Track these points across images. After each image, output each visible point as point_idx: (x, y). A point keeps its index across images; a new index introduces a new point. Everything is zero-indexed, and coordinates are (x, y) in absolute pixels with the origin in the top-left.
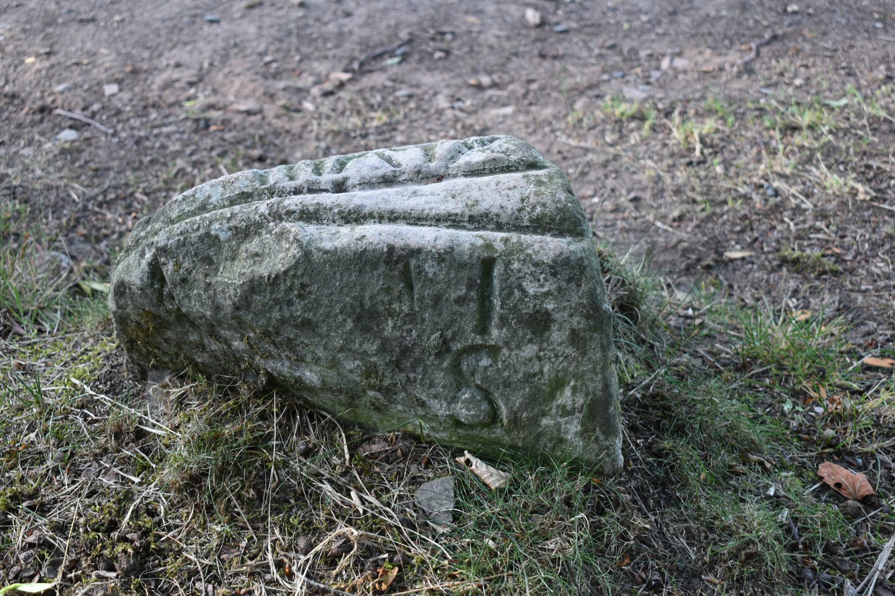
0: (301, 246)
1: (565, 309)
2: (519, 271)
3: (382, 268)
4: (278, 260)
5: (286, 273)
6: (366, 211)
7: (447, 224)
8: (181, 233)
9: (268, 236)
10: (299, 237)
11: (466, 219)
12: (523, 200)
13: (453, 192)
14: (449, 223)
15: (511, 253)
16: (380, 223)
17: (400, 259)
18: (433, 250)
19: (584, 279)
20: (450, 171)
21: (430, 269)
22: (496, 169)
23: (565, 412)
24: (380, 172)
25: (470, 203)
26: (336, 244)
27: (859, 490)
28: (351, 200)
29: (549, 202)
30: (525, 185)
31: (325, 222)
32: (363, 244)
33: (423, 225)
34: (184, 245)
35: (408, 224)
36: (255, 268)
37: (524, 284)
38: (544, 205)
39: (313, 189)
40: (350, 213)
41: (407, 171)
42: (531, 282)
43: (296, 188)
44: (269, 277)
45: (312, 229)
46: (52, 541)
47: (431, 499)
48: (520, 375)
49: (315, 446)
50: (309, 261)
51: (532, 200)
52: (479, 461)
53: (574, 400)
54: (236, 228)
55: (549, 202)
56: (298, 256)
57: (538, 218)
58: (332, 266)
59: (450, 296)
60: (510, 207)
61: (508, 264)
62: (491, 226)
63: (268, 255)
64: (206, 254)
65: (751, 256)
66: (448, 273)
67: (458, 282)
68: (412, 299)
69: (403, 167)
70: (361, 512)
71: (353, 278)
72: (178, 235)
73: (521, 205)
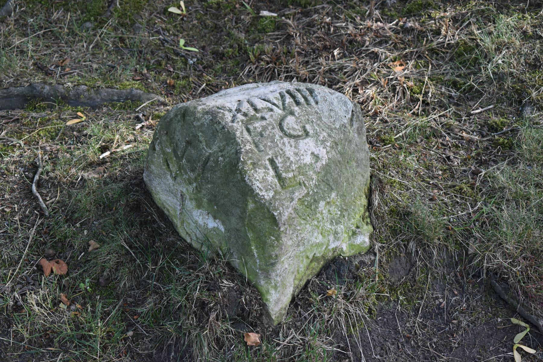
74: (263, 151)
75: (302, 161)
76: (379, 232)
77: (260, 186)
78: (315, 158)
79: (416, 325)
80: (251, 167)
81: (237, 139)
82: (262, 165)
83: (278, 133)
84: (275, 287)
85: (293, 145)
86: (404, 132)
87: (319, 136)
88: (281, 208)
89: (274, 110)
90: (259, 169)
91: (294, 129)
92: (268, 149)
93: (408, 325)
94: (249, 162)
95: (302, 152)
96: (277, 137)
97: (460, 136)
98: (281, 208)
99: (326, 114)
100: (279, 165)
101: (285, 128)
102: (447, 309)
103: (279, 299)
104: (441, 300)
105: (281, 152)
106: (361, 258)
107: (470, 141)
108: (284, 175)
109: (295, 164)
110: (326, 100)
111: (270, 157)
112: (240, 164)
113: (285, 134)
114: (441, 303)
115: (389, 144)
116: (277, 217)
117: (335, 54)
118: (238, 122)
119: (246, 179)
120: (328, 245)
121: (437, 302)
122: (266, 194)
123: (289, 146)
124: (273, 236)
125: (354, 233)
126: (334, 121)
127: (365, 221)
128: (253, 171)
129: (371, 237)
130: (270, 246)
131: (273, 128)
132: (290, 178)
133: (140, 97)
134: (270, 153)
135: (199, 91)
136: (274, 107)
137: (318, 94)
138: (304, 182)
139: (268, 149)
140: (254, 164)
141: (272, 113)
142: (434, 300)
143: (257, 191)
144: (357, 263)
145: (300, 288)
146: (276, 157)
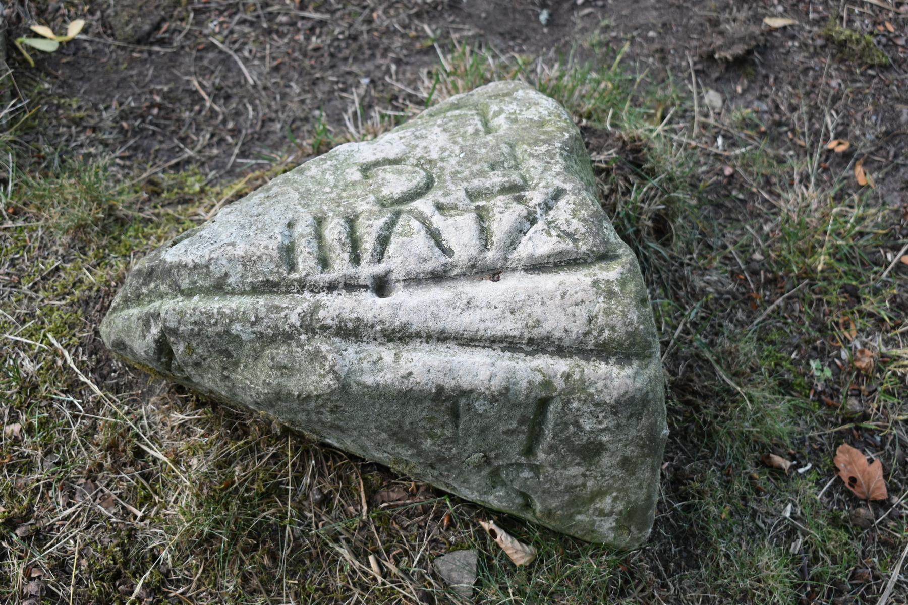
0: (338, 378)
1: (620, 440)
2: (578, 410)
3: (428, 403)
4: (310, 382)
5: (318, 396)
6: (413, 330)
7: (502, 346)
8: (195, 323)
9: (299, 350)
10: (336, 368)
11: (525, 341)
12: (590, 321)
13: (513, 306)
14: (505, 345)
15: (571, 391)
16: (428, 343)
17: (449, 398)
18: (487, 392)
19: (646, 412)
20: (509, 264)
21: (480, 406)
22: (561, 262)
23: (601, 513)
24: (429, 266)
25: (531, 323)
26: (378, 378)
27: (873, 492)
28: (396, 315)
29: (619, 325)
30: (593, 298)
31: (365, 339)
32: (409, 383)
33: (476, 346)
34: (199, 334)
35: (459, 344)
36: (283, 380)
37: (581, 421)
38: (613, 328)
39: (351, 286)
40: (394, 331)
41: (460, 264)
42: (589, 419)
43: (330, 283)
44: (299, 396)
45: (351, 351)
46: (54, 589)
47: (451, 570)
48: (562, 487)
49: (330, 492)
50: (347, 393)
51: (601, 320)
52: (504, 534)
53: (613, 506)
54: (261, 333)
55: (619, 325)
56: (334, 387)
57: (604, 343)
58: (371, 397)
59: (499, 428)
60: (575, 330)
61: (566, 403)
62: (550, 349)
63: (298, 370)
64: (224, 347)
65: (792, 26)
66: (500, 411)
67: (510, 418)
68: (457, 426)
69: (455, 257)
70: (380, 582)
71: (394, 407)
72: (191, 324)
73: (587, 328)
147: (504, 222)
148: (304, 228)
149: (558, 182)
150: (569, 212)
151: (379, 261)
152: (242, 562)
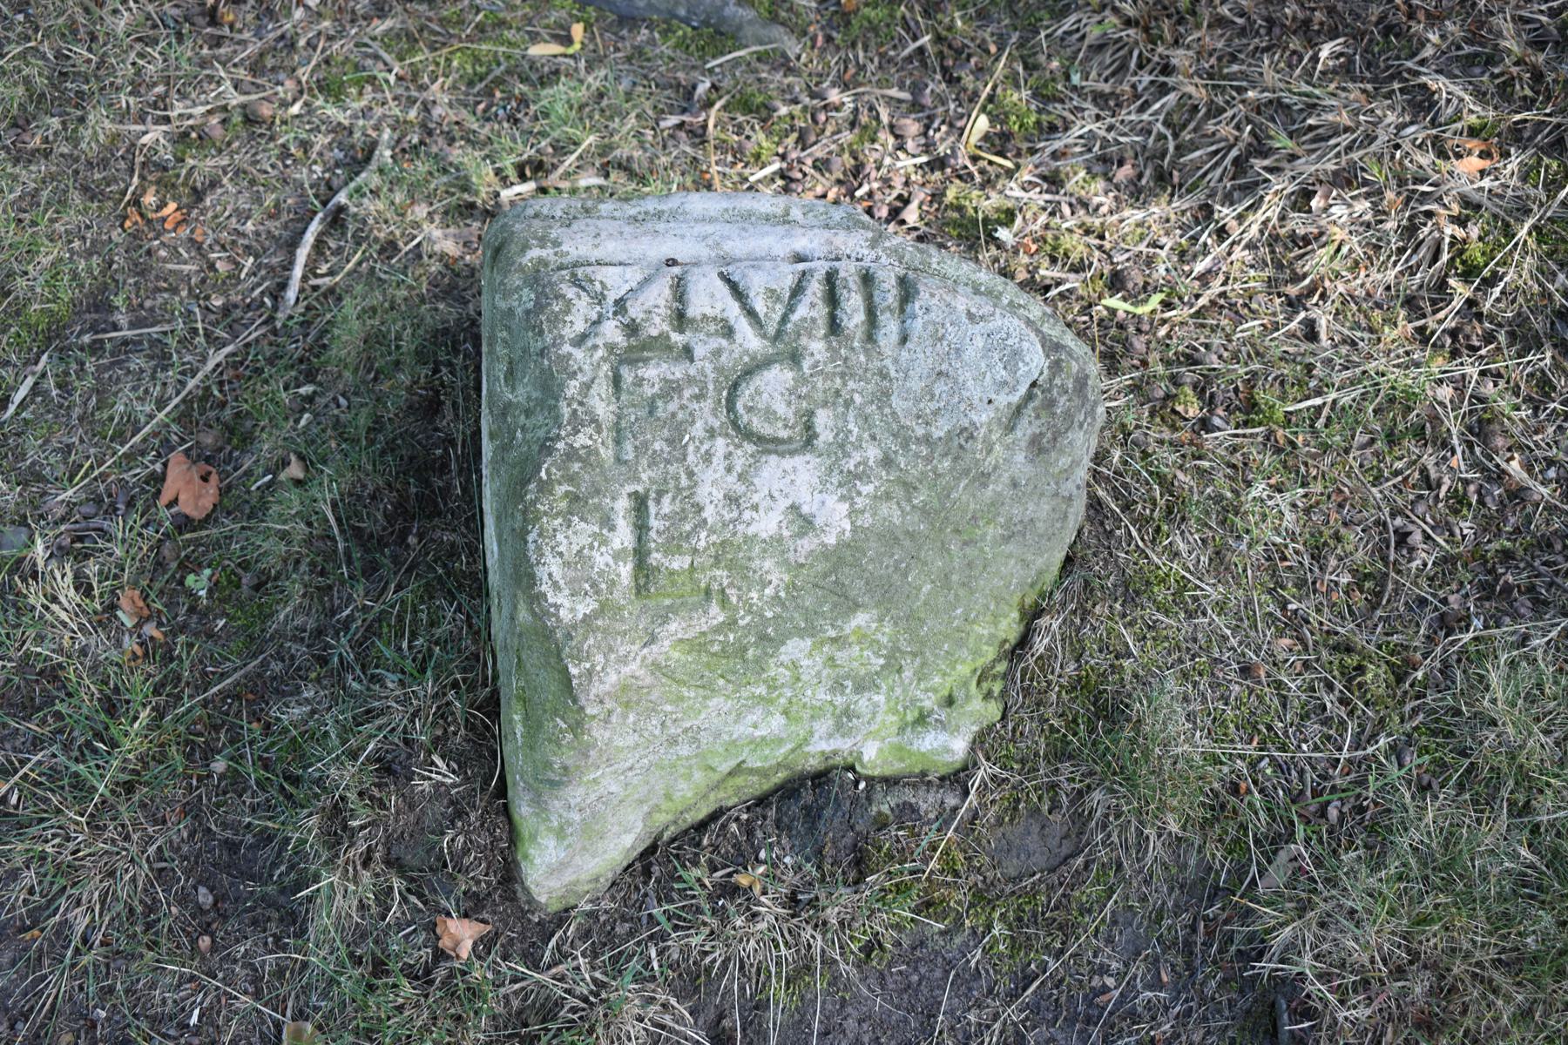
74: (626, 462)
75: (741, 528)
76: (1014, 730)
77: (557, 576)
78: (800, 522)
79: (997, 1026)
80: (563, 505)
81: (563, 404)
82: (598, 507)
83: (707, 415)
84: (560, 834)
85: (738, 469)
86: (1333, 395)
87: (847, 455)
88: (599, 658)
89: (738, 337)
90: (582, 519)
91: (770, 415)
92: (644, 462)
93: (972, 1018)
94: (560, 490)
95: (756, 498)
96: (698, 429)
97: (1497, 466)
98: (599, 658)
99: (916, 385)
100: (654, 523)
101: (739, 406)
102: (1111, 1013)
103: (563, 866)
104: (1110, 982)
105: (684, 482)
106: (908, 796)
107: (1517, 495)
108: (655, 558)
109: (712, 531)
110: (941, 339)
111: (640, 489)
112: (532, 486)
113: (735, 424)
114: (1105, 990)
115: (1260, 424)
116: (575, 682)
117: (1324, 54)
118: (595, 347)
119: (530, 538)
120: (806, 741)
121: (1096, 982)
122: (567, 604)
123: (721, 468)
124: (563, 719)
125: (922, 719)
126: (936, 413)
127: (985, 685)
128: (560, 520)
129: (979, 741)
130: (550, 741)
131: (699, 397)
132: (672, 573)
133: (740, 27)
134: (644, 477)
135: (906, 52)
136: (743, 326)
137: (920, 313)
138: (723, 591)
139: (644, 462)
140: (574, 498)
141: (724, 343)
142: (1093, 972)
143: (544, 588)
144: (885, 809)
145: (684, 826)
146: (660, 494)
147: (656, 293)
148: (890, 327)
149: (579, 354)
150: (574, 310)
151: (804, 273)
152: (984, 881)
